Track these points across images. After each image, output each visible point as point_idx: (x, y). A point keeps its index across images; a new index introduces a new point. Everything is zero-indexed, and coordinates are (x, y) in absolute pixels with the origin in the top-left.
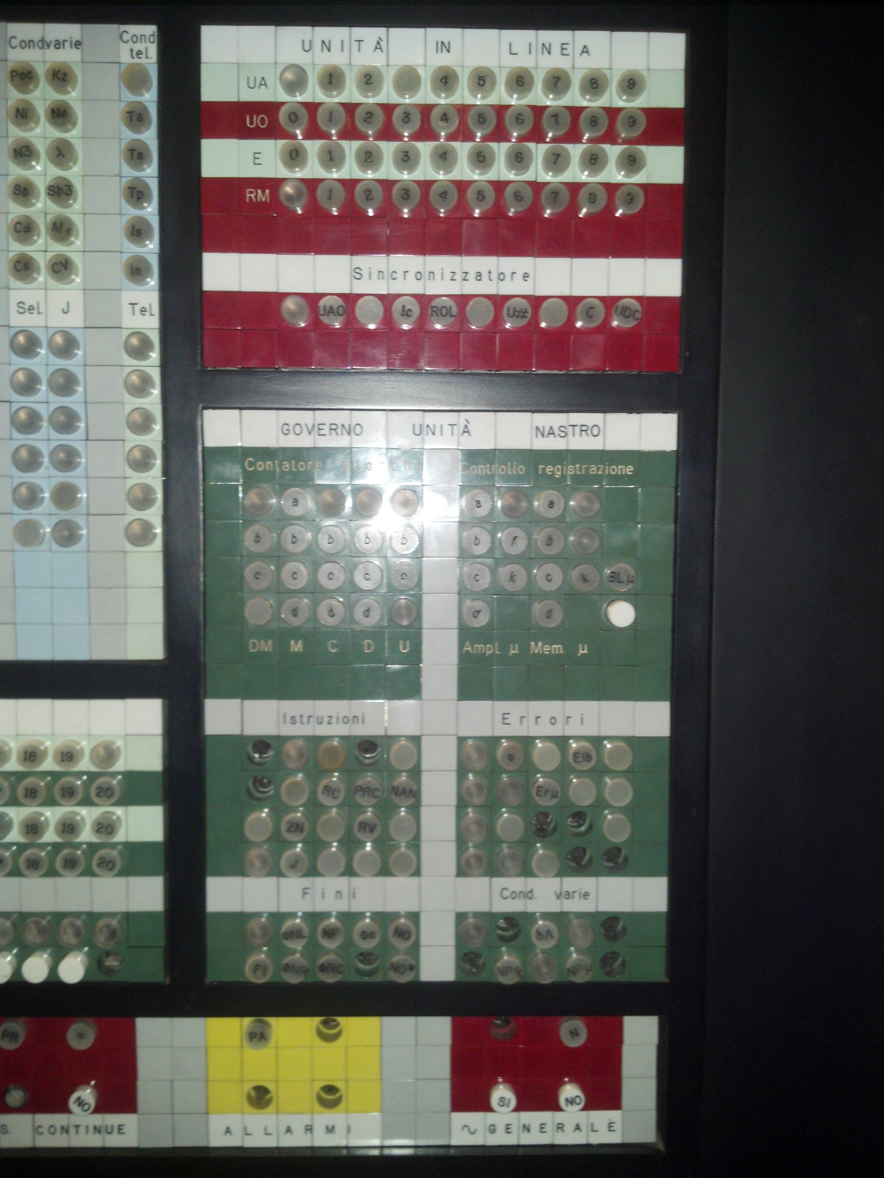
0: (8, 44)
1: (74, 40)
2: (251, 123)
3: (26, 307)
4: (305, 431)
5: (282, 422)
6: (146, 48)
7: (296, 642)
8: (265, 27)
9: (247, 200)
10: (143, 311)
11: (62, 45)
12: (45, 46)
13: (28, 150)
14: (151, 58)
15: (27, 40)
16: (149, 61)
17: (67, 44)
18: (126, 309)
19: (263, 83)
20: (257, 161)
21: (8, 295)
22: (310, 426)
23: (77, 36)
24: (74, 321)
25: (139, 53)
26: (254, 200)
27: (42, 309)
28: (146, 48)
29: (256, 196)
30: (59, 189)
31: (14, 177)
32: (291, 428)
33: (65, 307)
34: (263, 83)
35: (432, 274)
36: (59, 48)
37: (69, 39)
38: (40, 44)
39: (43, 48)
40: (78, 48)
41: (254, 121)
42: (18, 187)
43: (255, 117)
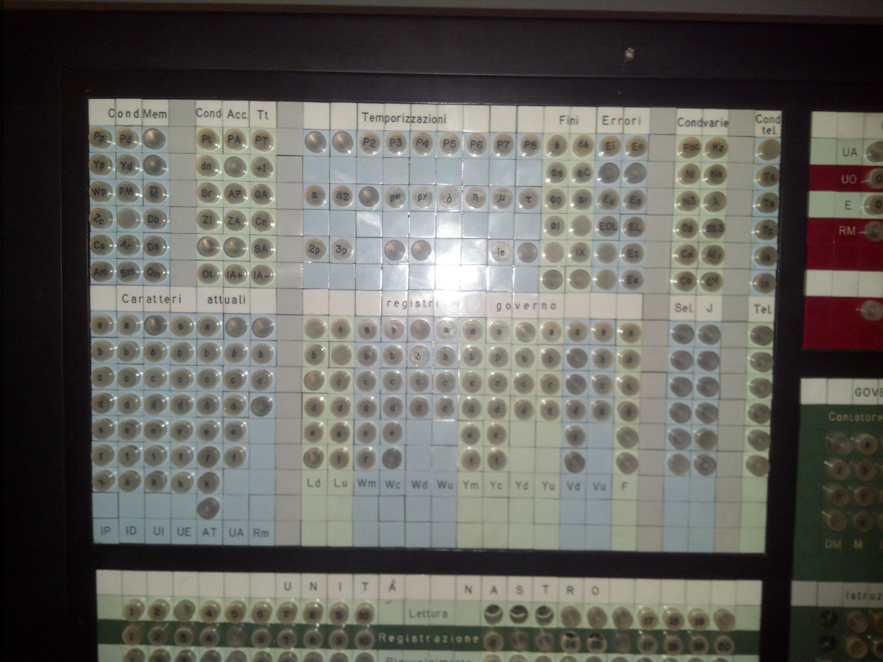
0: (677, 123)
1: (724, 121)
2: (845, 180)
3: (682, 307)
4: (872, 394)
5: (855, 387)
6: (774, 127)
7: (858, 542)
8: (819, 112)
9: (840, 234)
10: (764, 310)
11: (715, 124)
12: (703, 125)
13: (693, 200)
14: (777, 134)
15: (691, 120)
16: (775, 136)
17: (719, 124)
18: (752, 309)
19: (854, 152)
20: (848, 207)
21: (669, 298)
22: (875, 390)
23: (726, 119)
24: (715, 317)
25: (769, 130)
26: (845, 234)
27: (693, 308)
28: (774, 127)
29: (846, 231)
30: (714, 227)
31: (202, 129)
32: (862, 391)
33: (709, 307)
34: (854, 152)
35: (128, 113)
36: (713, 126)
37: (638, 118)
38: (387, 120)
39: (701, 126)
40: (726, 127)
41: (846, 179)
42: (685, 226)
43: (848, 176)
